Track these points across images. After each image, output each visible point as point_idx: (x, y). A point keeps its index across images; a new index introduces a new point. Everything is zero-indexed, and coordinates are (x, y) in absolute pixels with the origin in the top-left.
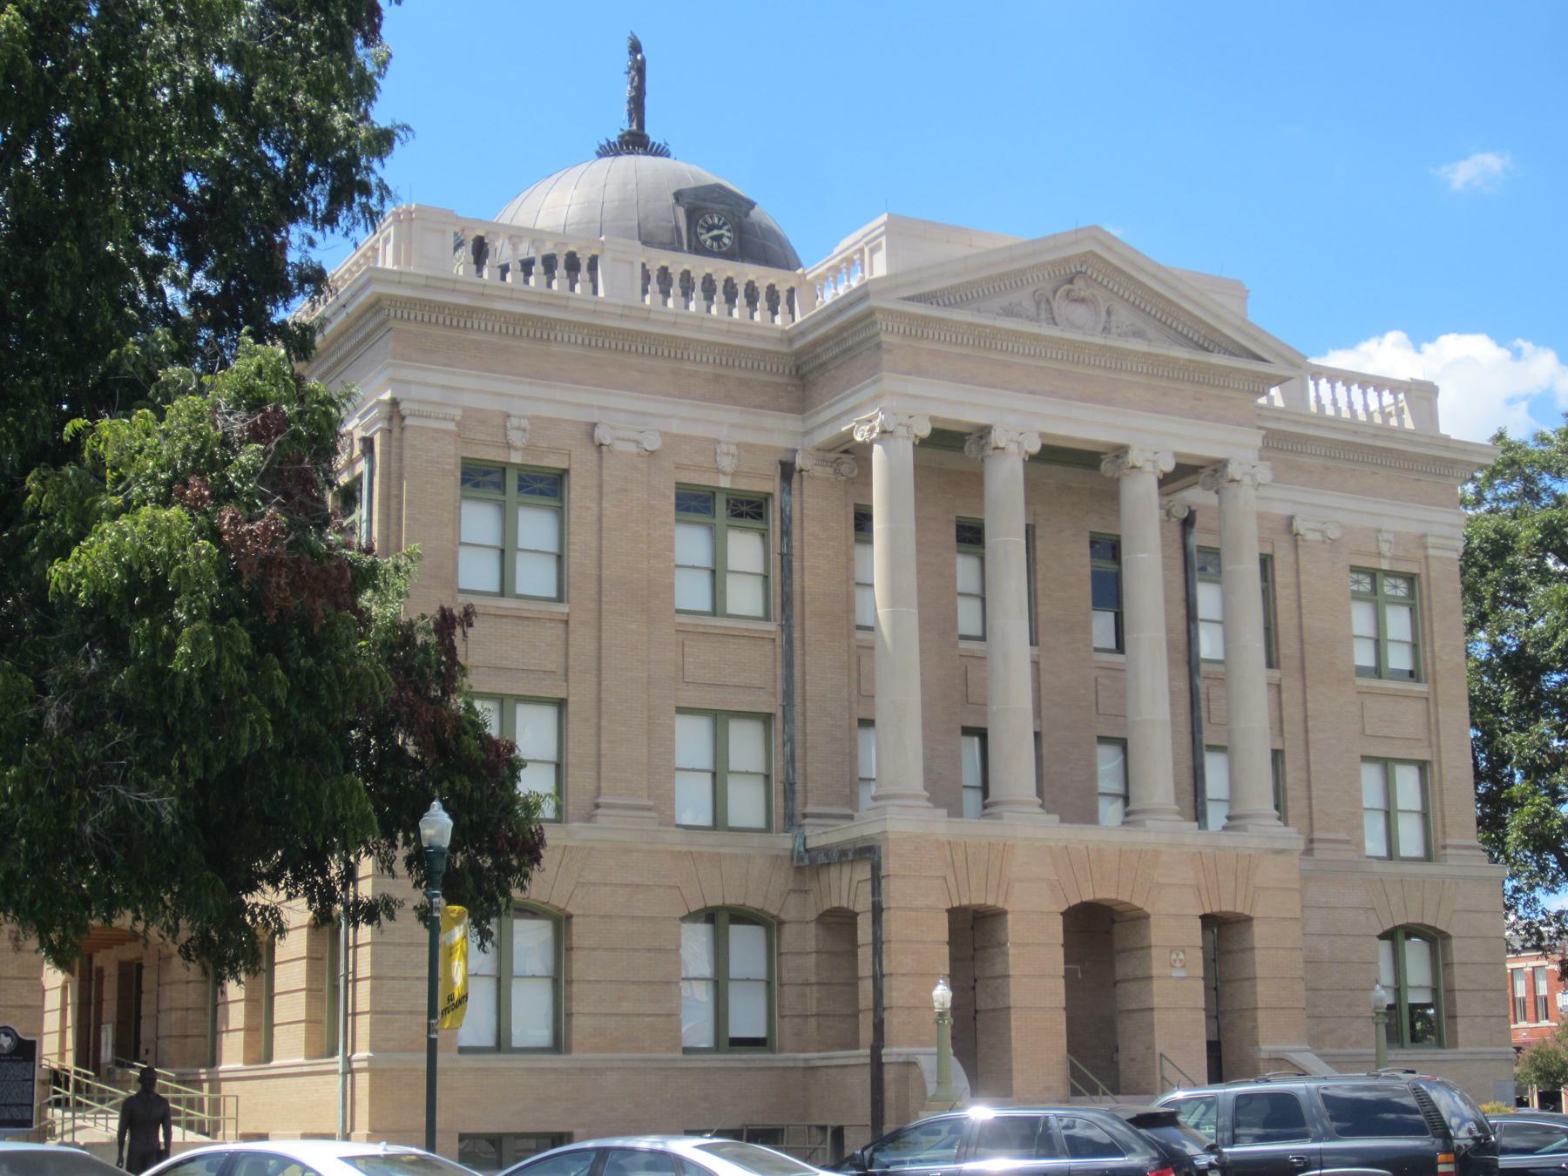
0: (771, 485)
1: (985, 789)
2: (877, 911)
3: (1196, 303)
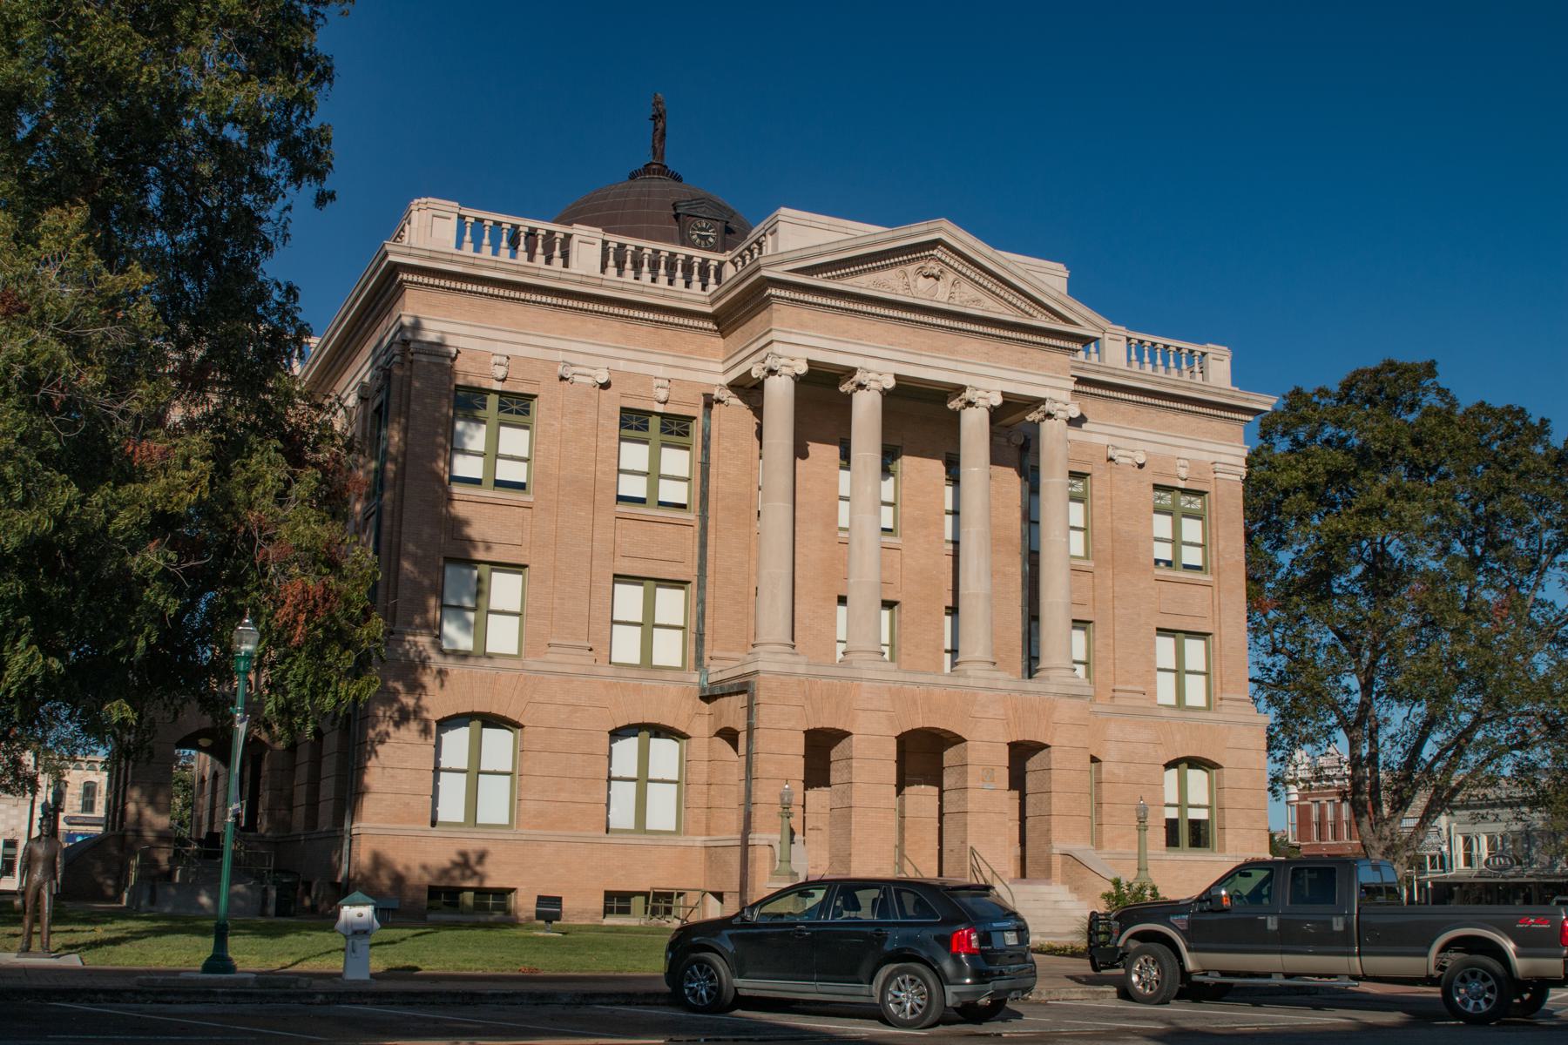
0: (698, 412)
1: (954, 652)
2: (750, 730)
3: (1023, 280)
